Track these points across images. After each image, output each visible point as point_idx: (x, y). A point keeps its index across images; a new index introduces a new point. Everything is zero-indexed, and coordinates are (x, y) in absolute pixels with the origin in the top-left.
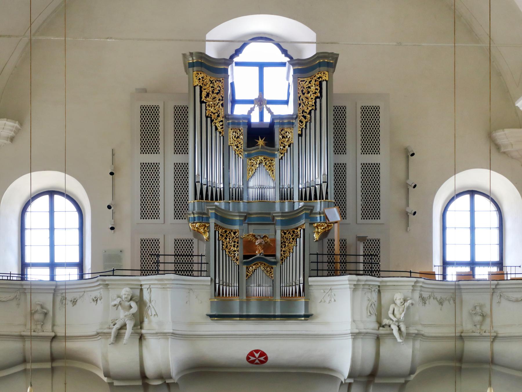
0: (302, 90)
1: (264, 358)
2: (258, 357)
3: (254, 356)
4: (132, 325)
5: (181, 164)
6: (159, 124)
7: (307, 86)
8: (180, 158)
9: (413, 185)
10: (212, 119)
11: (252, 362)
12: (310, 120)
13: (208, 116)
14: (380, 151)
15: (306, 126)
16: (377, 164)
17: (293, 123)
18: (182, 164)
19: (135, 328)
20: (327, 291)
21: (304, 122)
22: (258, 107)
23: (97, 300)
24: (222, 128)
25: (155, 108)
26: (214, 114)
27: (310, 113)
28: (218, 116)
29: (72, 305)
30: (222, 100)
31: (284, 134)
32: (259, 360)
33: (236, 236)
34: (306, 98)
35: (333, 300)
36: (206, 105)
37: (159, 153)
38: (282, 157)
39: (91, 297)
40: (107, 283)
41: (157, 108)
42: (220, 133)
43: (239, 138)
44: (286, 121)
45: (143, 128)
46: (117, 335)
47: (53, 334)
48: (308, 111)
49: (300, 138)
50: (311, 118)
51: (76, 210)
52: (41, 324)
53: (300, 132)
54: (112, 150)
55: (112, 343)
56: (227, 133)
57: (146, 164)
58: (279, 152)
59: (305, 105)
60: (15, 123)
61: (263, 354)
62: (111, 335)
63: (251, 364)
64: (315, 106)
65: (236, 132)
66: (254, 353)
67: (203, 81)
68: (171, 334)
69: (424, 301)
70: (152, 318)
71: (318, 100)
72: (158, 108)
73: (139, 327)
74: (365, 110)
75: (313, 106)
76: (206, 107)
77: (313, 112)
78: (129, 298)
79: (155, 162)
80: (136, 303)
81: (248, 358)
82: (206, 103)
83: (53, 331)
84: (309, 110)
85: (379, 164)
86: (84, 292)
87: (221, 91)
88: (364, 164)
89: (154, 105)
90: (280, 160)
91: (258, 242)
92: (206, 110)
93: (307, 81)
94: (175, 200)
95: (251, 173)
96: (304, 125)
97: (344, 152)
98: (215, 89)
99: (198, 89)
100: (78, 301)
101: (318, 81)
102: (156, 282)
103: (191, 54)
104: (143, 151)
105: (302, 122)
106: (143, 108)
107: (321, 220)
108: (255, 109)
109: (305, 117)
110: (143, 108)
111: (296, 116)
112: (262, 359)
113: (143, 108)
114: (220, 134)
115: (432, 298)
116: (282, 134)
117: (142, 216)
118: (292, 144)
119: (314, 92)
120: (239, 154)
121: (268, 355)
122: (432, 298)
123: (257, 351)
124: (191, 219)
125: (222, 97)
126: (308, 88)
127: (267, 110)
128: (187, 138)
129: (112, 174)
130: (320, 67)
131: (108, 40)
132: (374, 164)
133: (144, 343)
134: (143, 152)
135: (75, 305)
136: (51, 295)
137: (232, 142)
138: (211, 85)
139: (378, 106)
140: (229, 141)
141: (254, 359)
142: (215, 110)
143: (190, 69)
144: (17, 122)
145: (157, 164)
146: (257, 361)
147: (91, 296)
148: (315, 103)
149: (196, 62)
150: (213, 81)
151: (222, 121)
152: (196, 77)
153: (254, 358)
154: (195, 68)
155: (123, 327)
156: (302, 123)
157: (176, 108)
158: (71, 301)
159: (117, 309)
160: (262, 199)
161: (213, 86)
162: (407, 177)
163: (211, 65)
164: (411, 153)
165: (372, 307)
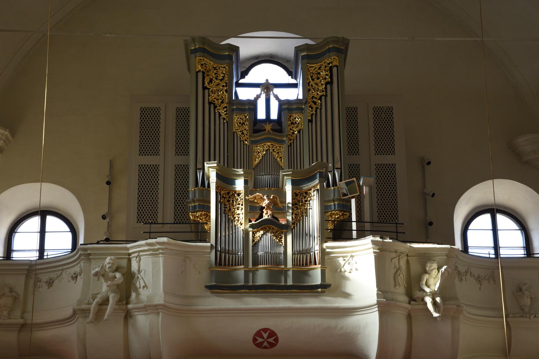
0: (311, 75)
1: (274, 340)
2: (267, 339)
3: (262, 337)
4: (117, 299)
5: (182, 166)
6: (160, 125)
7: (316, 73)
8: (180, 160)
9: (431, 194)
10: (216, 105)
11: (259, 345)
12: (320, 106)
13: (211, 102)
14: (396, 152)
15: (316, 111)
16: (392, 165)
17: (302, 109)
18: (184, 166)
19: (120, 303)
20: (347, 259)
21: (314, 108)
22: (264, 94)
23: (76, 277)
24: (226, 114)
25: (156, 110)
26: (217, 100)
27: (320, 99)
28: (222, 102)
29: (47, 287)
30: (226, 86)
31: (293, 120)
32: (268, 342)
33: (240, 198)
34: (315, 83)
35: (354, 269)
36: (209, 91)
37: (159, 155)
38: (291, 144)
39: (70, 275)
40: (89, 252)
41: (158, 110)
42: (224, 119)
43: (245, 124)
44: (294, 107)
45: (143, 126)
46: (98, 312)
47: (21, 321)
48: (318, 97)
49: (310, 123)
50: (321, 104)
51: (69, 230)
52: (8, 309)
53: (310, 118)
54: (110, 161)
55: (91, 322)
56: (232, 119)
57: (145, 166)
58: (288, 138)
59: (315, 91)
60: (6, 131)
61: (272, 334)
62: (90, 312)
63: (257, 348)
64: (326, 92)
65: (241, 118)
66: (262, 332)
67: (206, 67)
68: (162, 307)
69: (460, 277)
70: (141, 290)
71: (328, 86)
72: (159, 110)
73: (124, 302)
74: (378, 111)
75: (323, 91)
76: (209, 93)
77: (323, 98)
78: (114, 268)
79: (154, 164)
80: (123, 275)
81: (255, 340)
82: (209, 89)
83: (22, 318)
84: (319, 96)
85: (395, 165)
86: (63, 270)
87: (225, 77)
88: (378, 165)
89: (155, 106)
90: (289, 146)
91: (265, 203)
92: (209, 96)
93: (316, 68)
94: (175, 203)
95: (257, 159)
96: (314, 110)
97: (357, 153)
98: (219, 75)
99: (200, 75)
100: (55, 281)
101: (328, 66)
102: (146, 248)
103: (193, 40)
104: (143, 152)
105: (312, 108)
106: (143, 111)
107: (335, 208)
108: (261, 96)
109: (315, 103)
110: (143, 109)
111: (305, 101)
112: (271, 340)
113: (143, 109)
114: (224, 120)
115: (469, 274)
116: (291, 121)
117: (139, 220)
118: (301, 131)
119: (324, 78)
120: (244, 141)
121: (279, 335)
122: (469, 274)
123: (265, 330)
124: (191, 208)
125: (226, 83)
126: (318, 74)
127: (274, 97)
128: (188, 142)
129: (108, 183)
130: (329, 52)
131: (107, 35)
132: (390, 165)
133: (131, 321)
134: (141, 154)
135: (51, 287)
136: (23, 277)
137: (236, 128)
138: (215, 71)
139: (391, 107)
140: (234, 125)
141: (262, 340)
142: (219, 96)
143: (192, 55)
144: (8, 130)
145: (156, 166)
146: (265, 344)
147: (70, 274)
148: (326, 88)
149: (198, 48)
150: (216, 67)
151: (226, 107)
152: (199, 62)
153: (262, 340)
154: (198, 54)
155: (105, 301)
156: (311, 109)
157: (178, 110)
158: (46, 282)
159: (98, 280)
160: (270, 187)
161: (217, 73)
162: (424, 187)
163: (215, 53)
164: (427, 161)
165: (400, 277)
